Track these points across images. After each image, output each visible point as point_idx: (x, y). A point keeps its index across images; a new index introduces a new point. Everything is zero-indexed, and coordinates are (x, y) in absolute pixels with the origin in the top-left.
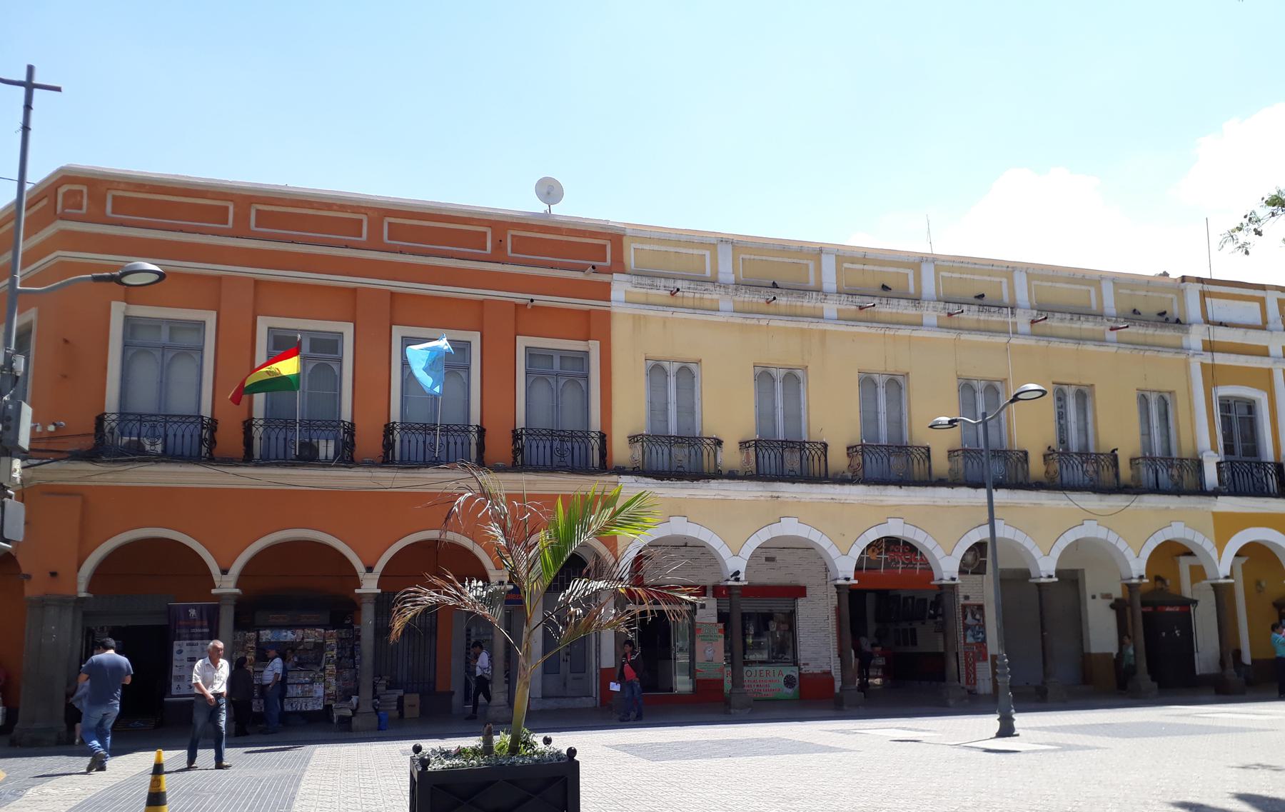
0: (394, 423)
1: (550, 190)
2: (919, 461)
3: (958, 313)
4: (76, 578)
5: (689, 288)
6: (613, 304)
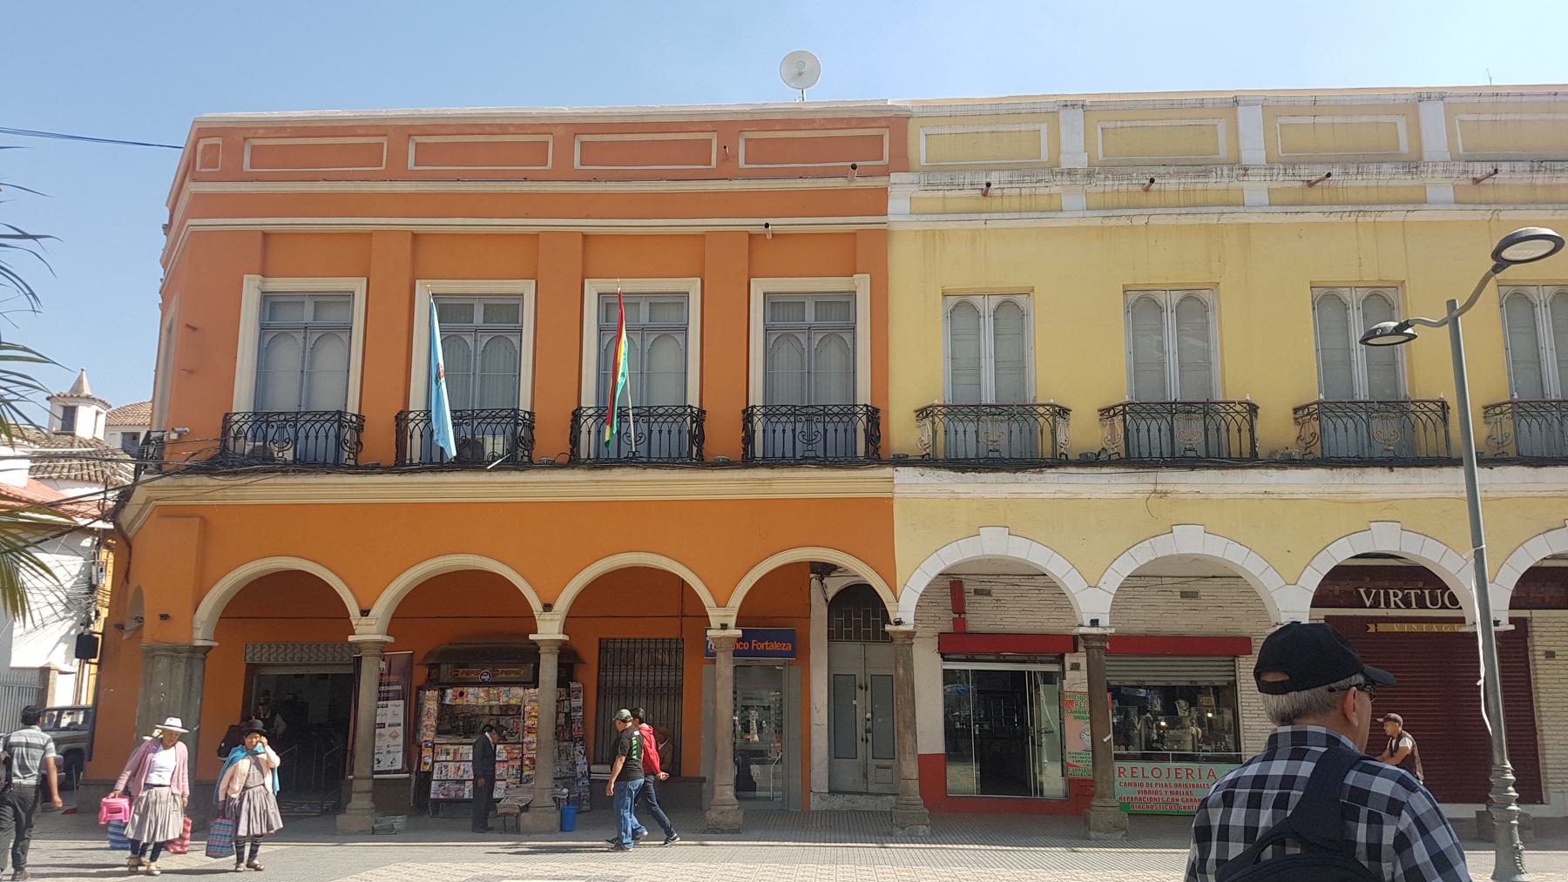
0: (754, 407)
1: (801, 69)
3: (1489, 175)
4: (192, 621)
5: (1011, 182)
6: (890, 218)
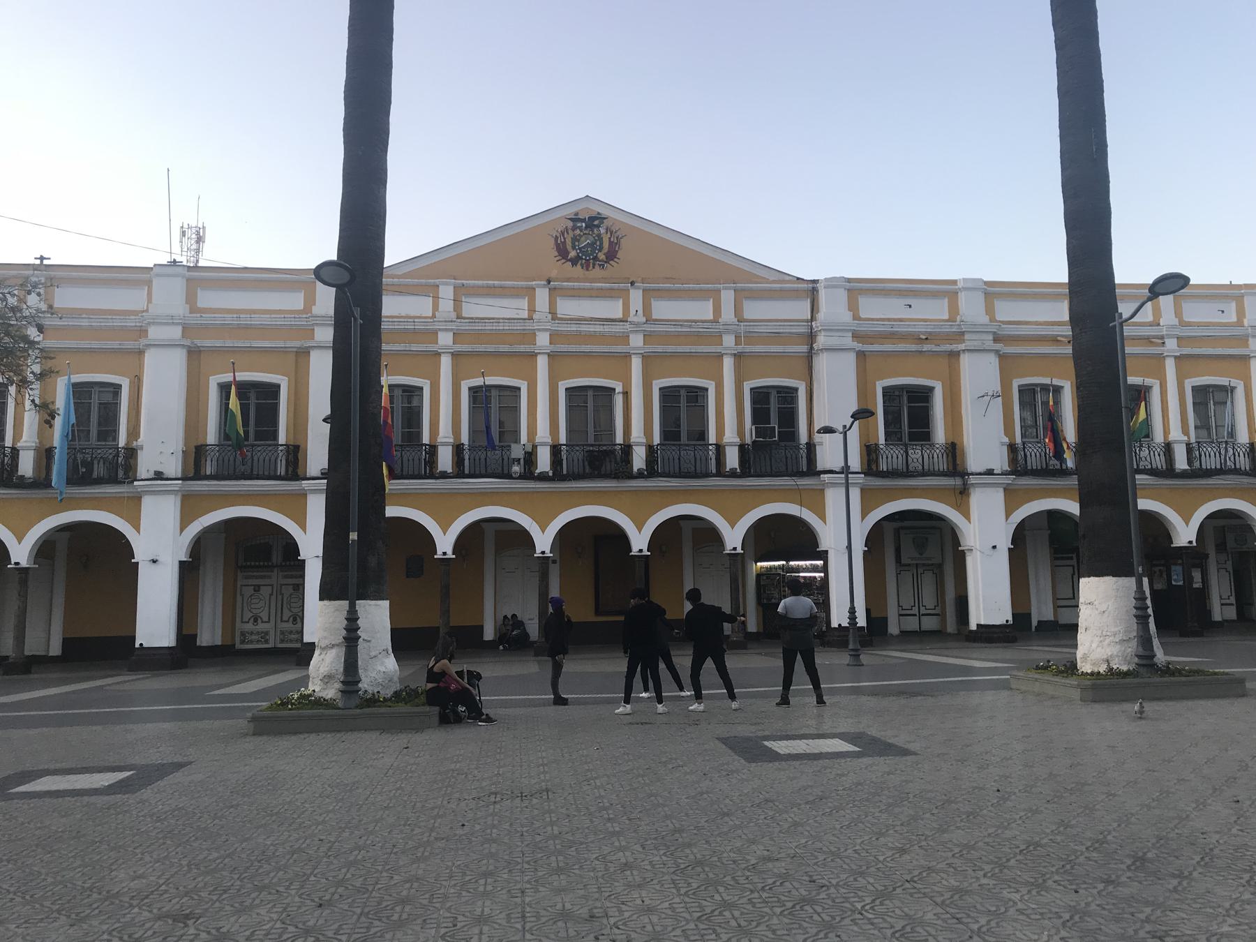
2: (1215, 454)
